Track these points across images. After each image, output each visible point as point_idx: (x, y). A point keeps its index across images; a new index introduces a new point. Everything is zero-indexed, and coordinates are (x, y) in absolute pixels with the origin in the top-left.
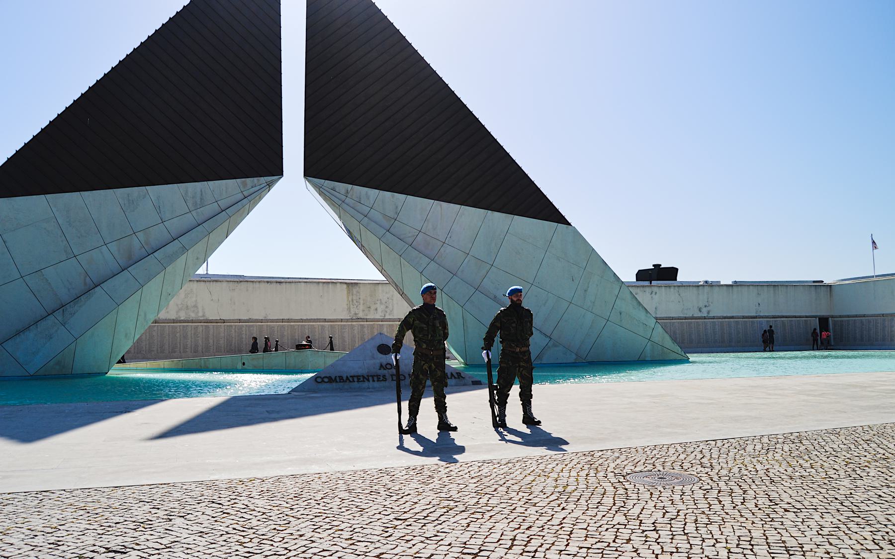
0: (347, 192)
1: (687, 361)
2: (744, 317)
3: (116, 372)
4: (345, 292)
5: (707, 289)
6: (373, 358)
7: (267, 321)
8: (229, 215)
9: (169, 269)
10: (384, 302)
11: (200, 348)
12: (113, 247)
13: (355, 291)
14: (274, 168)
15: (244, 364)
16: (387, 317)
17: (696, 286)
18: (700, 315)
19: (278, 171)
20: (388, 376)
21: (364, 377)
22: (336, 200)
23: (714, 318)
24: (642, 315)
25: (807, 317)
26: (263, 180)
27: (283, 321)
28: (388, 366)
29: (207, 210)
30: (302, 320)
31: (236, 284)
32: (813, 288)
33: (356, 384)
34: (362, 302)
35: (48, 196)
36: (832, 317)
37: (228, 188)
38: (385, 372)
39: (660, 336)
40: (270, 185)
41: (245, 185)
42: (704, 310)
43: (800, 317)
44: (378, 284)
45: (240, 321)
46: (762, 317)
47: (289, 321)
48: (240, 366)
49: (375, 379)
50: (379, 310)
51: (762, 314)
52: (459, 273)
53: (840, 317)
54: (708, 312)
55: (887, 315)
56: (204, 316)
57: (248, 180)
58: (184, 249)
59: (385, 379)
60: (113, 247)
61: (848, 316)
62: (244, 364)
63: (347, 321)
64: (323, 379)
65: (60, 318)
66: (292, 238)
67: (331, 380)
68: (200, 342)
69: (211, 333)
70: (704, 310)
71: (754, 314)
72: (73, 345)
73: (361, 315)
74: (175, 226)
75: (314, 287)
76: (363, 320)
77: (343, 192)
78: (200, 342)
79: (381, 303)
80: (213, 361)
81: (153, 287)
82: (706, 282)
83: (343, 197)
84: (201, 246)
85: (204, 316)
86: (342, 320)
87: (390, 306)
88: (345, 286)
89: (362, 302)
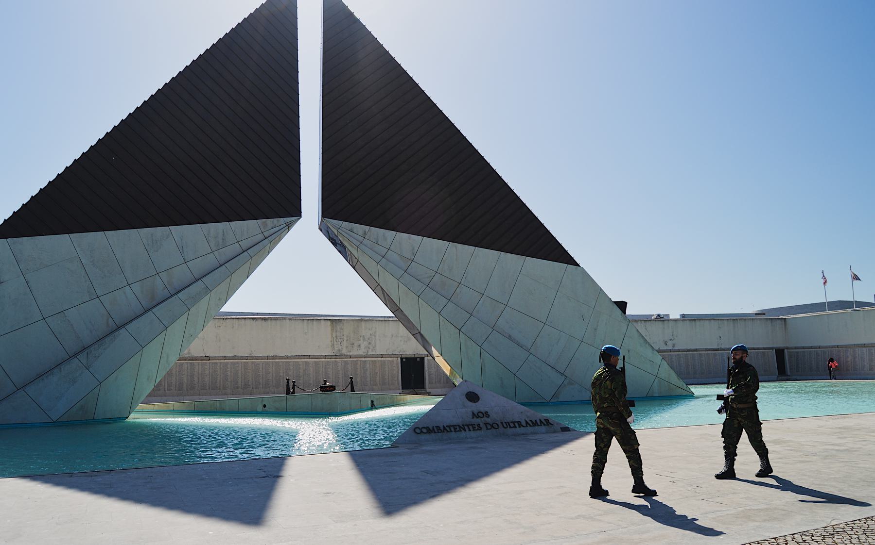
0: (365, 233)
1: (691, 396)
2: (707, 350)
3: (138, 417)
4: (329, 329)
5: (659, 324)
6: (464, 406)
7: (253, 358)
8: (248, 257)
9: (193, 310)
10: (366, 338)
11: (185, 386)
12: (136, 287)
13: (338, 328)
14: (292, 209)
15: (265, 406)
16: (370, 353)
17: (646, 319)
18: (665, 348)
19: (295, 211)
20: (482, 425)
21: (460, 427)
22: (355, 241)
23: (679, 351)
24: (648, 353)
25: (764, 349)
26: (282, 221)
27: (268, 357)
28: (481, 415)
29: (229, 251)
30: (287, 357)
31: (222, 321)
32: (769, 322)
33: (453, 434)
34: (345, 338)
35: (72, 235)
36: (788, 348)
37: (247, 229)
38: (478, 421)
39: (666, 372)
40: (289, 226)
41: (265, 225)
42: (670, 343)
43: (758, 349)
44: (385, 320)
45: (225, 358)
46: (724, 350)
47: (274, 357)
48: (260, 408)
49: (471, 427)
50: (363, 346)
51: (723, 347)
52: (475, 313)
53: (796, 348)
54: (674, 346)
55: (842, 346)
56: (189, 353)
57: (269, 221)
58: (208, 290)
59: (480, 429)
60: (136, 287)
61: (803, 348)
62: (265, 406)
63: (331, 357)
64: (421, 429)
65: (84, 362)
66: (304, 277)
67: (430, 431)
68: (185, 380)
69: (196, 370)
70: (670, 343)
71: (716, 347)
72: (98, 389)
73: (344, 352)
74: (198, 266)
75: (299, 324)
76: (346, 356)
77: (361, 233)
78: (185, 380)
79: (364, 339)
80: (231, 401)
81: (177, 327)
82: (683, 316)
83: (361, 239)
84: (224, 286)
85: (189, 353)
86: (326, 357)
87: (373, 343)
88: (329, 323)
89: (345, 338)
